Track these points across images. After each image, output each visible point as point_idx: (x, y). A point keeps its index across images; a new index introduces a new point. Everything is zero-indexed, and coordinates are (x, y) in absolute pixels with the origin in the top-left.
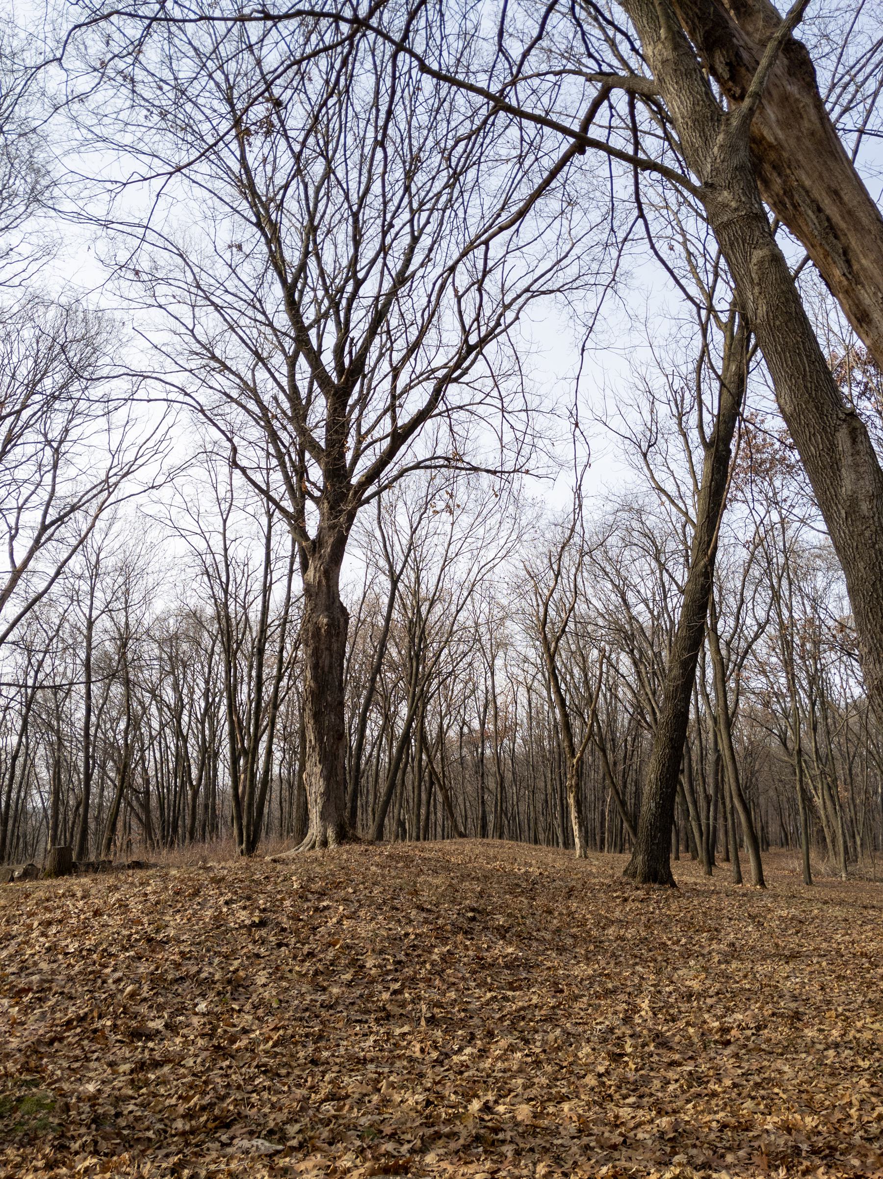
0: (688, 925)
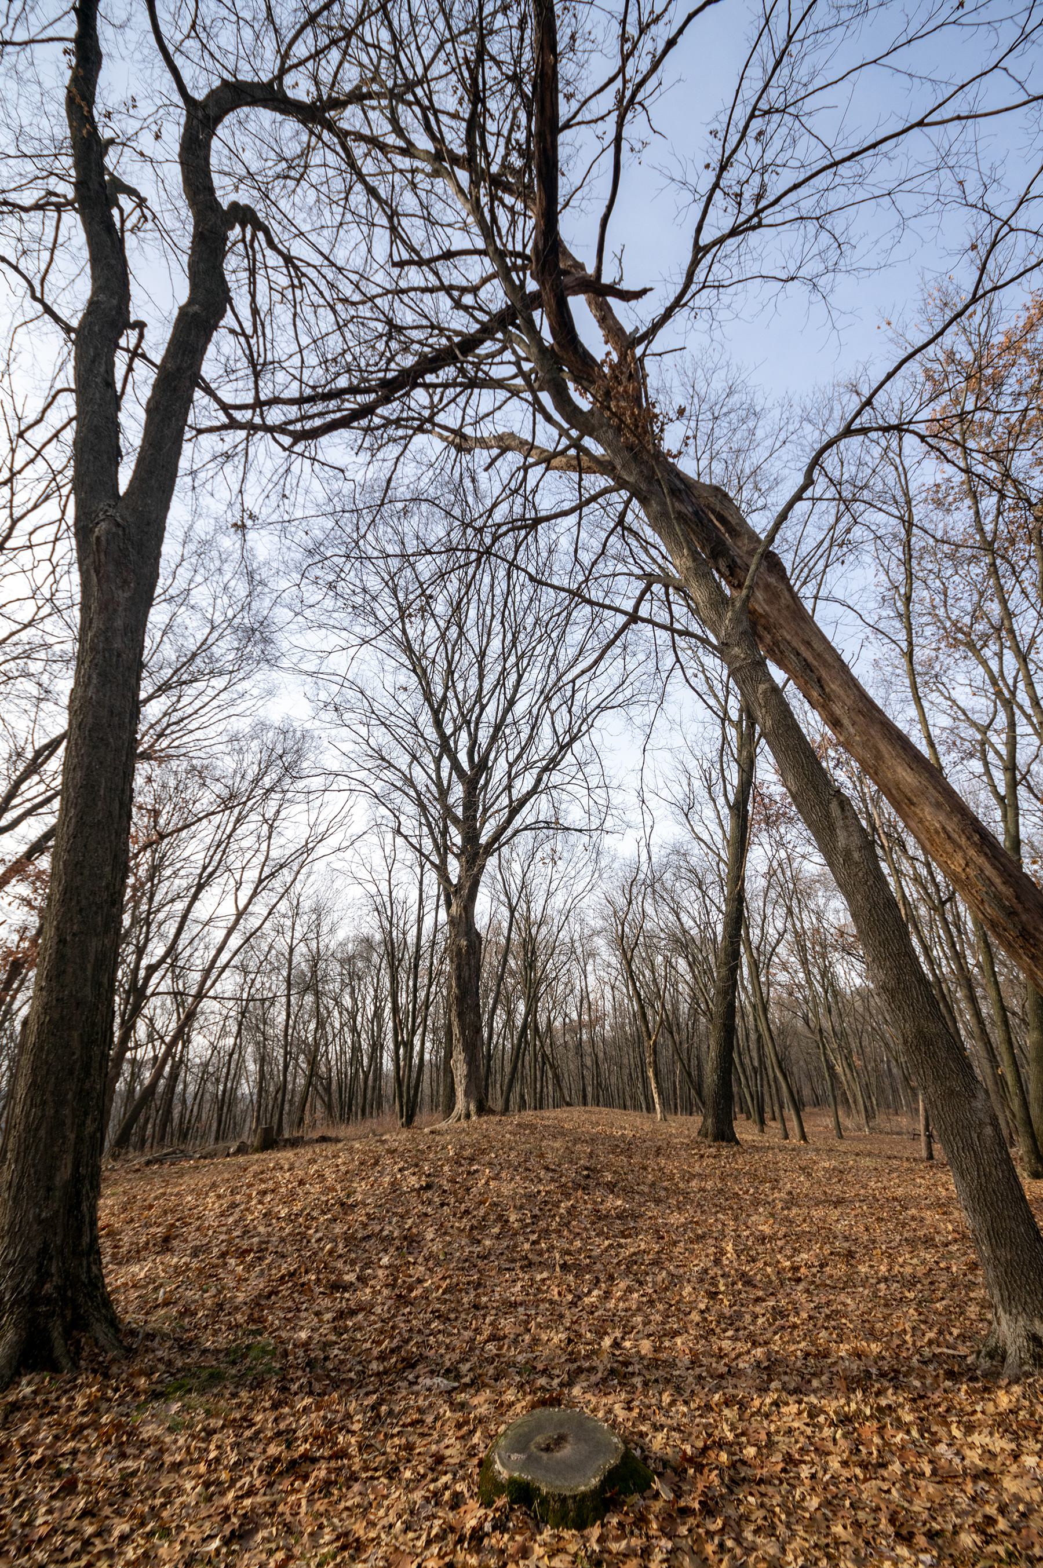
0: (753, 1176)
